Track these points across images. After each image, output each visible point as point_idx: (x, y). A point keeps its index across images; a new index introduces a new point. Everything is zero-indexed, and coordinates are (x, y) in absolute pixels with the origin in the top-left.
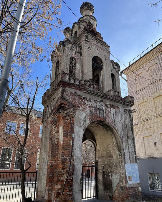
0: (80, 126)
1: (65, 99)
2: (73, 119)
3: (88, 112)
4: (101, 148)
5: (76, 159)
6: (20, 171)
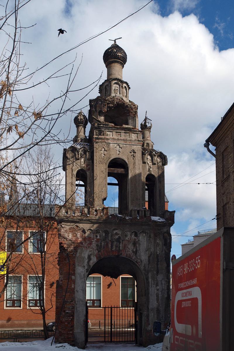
0: (82, 266)
1: (64, 238)
2: (75, 259)
3: (95, 248)
4: (114, 241)
5: (78, 301)
6: (2, 121)
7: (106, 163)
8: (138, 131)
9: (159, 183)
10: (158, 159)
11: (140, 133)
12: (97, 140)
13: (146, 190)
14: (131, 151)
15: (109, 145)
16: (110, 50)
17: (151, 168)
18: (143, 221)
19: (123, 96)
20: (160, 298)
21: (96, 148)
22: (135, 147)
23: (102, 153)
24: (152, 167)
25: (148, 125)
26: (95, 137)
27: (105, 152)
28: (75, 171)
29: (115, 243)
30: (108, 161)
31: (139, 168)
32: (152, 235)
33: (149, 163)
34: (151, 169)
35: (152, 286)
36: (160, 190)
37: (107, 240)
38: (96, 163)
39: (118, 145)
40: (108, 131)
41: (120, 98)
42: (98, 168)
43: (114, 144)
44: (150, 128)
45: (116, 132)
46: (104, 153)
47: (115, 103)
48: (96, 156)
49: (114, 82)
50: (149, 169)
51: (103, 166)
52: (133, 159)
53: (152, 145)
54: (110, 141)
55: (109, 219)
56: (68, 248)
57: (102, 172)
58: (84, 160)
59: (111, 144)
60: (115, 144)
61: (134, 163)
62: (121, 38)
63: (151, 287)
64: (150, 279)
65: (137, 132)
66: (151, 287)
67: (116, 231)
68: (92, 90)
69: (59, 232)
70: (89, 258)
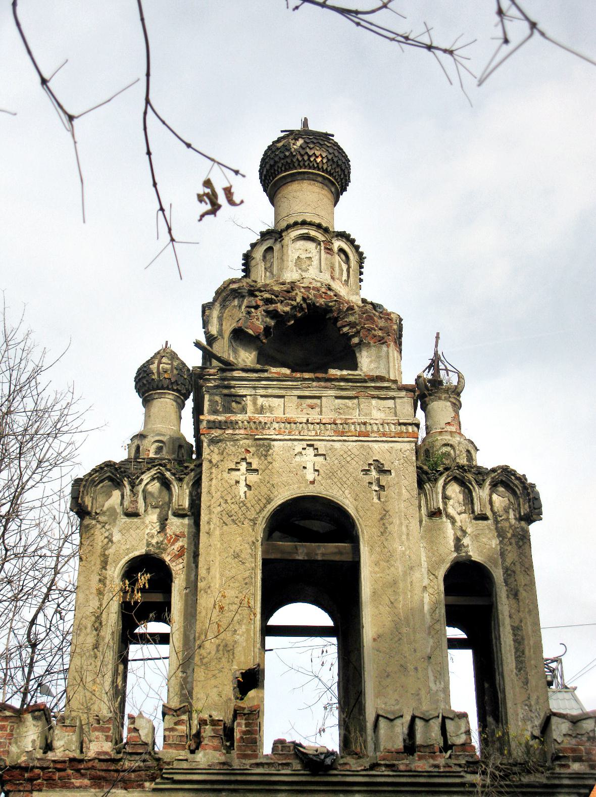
7: (254, 521)
8: (394, 386)
9: (508, 597)
10: (495, 497)
11: (403, 393)
12: (216, 433)
13: (454, 644)
14: (370, 465)
15: (269, 447)
16: (280, 145)
17: (464, 532)
19: (333, 278)
21: (210, 462)
22: (379, 450)
23: (237, 482)
24: (469, 530)
26: (209, 422)
27: (253, 478)
28: (116, 562)
30: (262, 510)
31: (408, 534)
33: (457, 518)
34: (466, 541)
38: (208, 523)
39: (308, 445)
40: (262, 396)
41: (319, 285)
42: (216, 540)
43: (289, 443)
44: (456, 392)
45: (300, 397)
46: (246, 480)
47: (299, 299)
48: (209, 492)
49: (295, 233)
50: (458, 540)
51: (240, 531)
52: (379, 499)
53: (468, 451)
54: (270, 433)
57: (236, 556)
58: (159, 515)
59: (275, 443)
60: (296, 443)
61: (384, 516)
62: (438, 334)
65: (391, 394)
68: (149, 153)
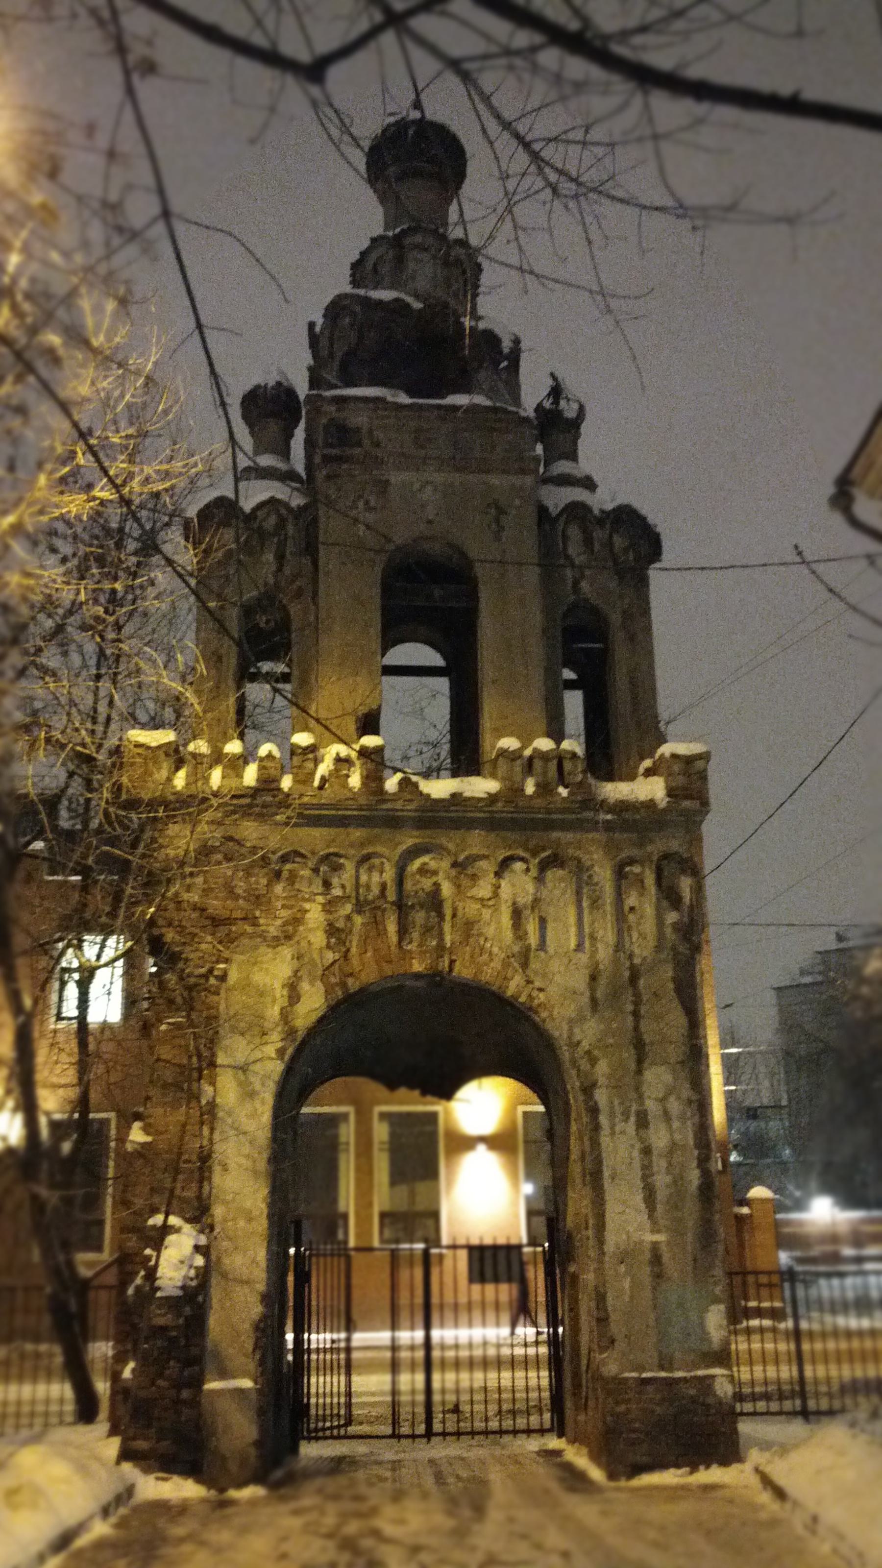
13: (570, 685)
18: (552, 806)
20: (661, 1195)
25: (569, 411)
29: (419, 917)
32: (604, 874)
35: (618, 1129)
36: (633, 683)
37: (145, 880)
55: (388, 800)
56: (184, 944)
63: (613, 1133)
64: (604, 1090)
66: (613, 1133)
67: (425, 859)
69: (417, 907)
70: (294, 994)
